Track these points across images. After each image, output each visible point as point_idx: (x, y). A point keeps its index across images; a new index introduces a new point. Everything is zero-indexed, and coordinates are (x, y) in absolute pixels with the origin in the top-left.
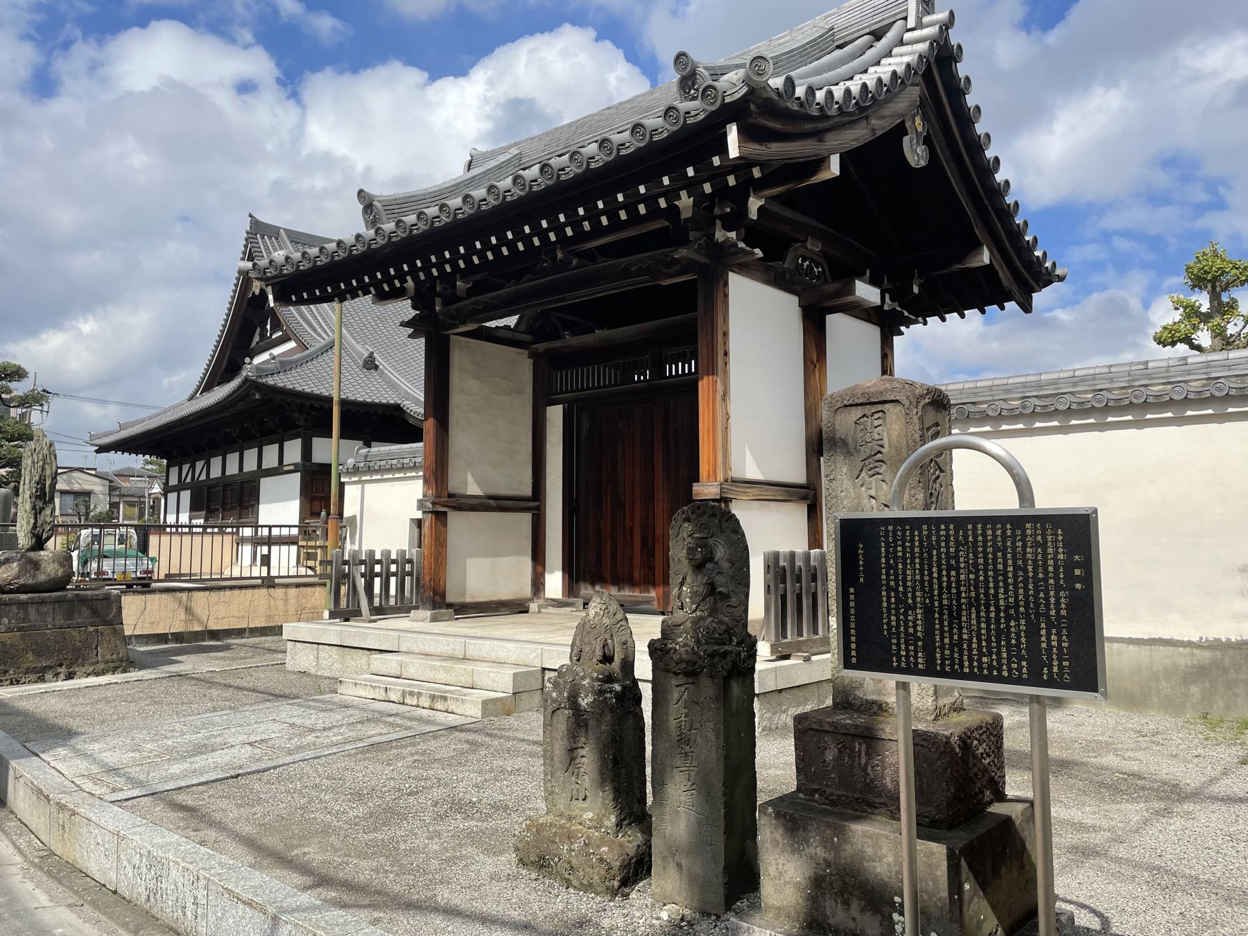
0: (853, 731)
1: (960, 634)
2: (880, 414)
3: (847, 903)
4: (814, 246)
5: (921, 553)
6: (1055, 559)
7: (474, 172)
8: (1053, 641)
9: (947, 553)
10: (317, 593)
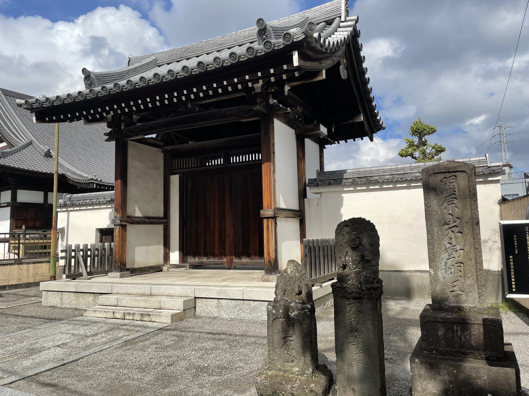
0: (454, 321)
2: (454, 177)
7: (131, 67)
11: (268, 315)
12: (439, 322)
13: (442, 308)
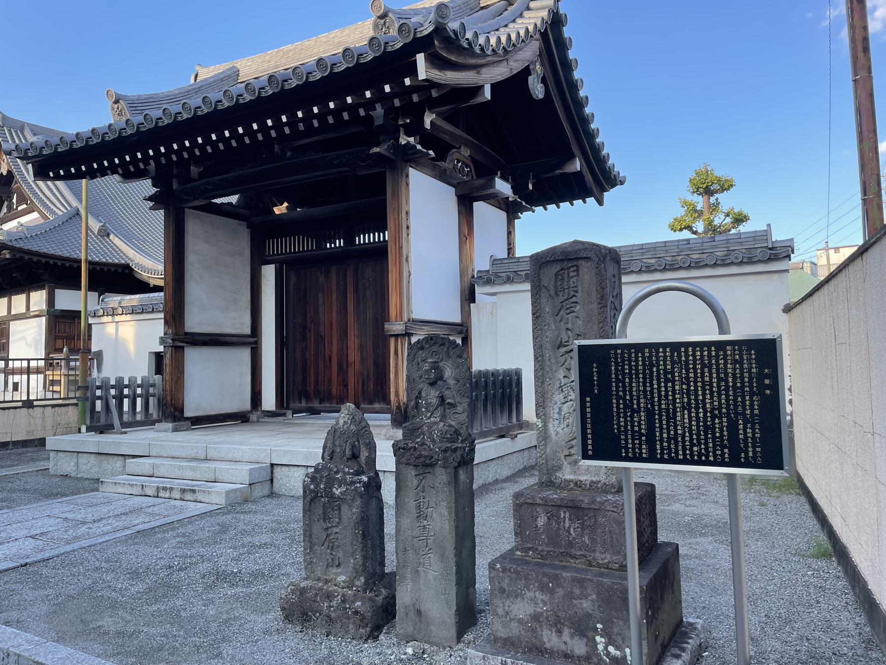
0: (559, 503)
1: (676, 430)
3: (560, 632)
4: (466, 152)
5: (644, 370)
6: (750, 372)
8: (747, 433)
9: (665, 369)
10: (70, 412)
11: (305, 492)
12: (539, 505)
13: (551, 482)
